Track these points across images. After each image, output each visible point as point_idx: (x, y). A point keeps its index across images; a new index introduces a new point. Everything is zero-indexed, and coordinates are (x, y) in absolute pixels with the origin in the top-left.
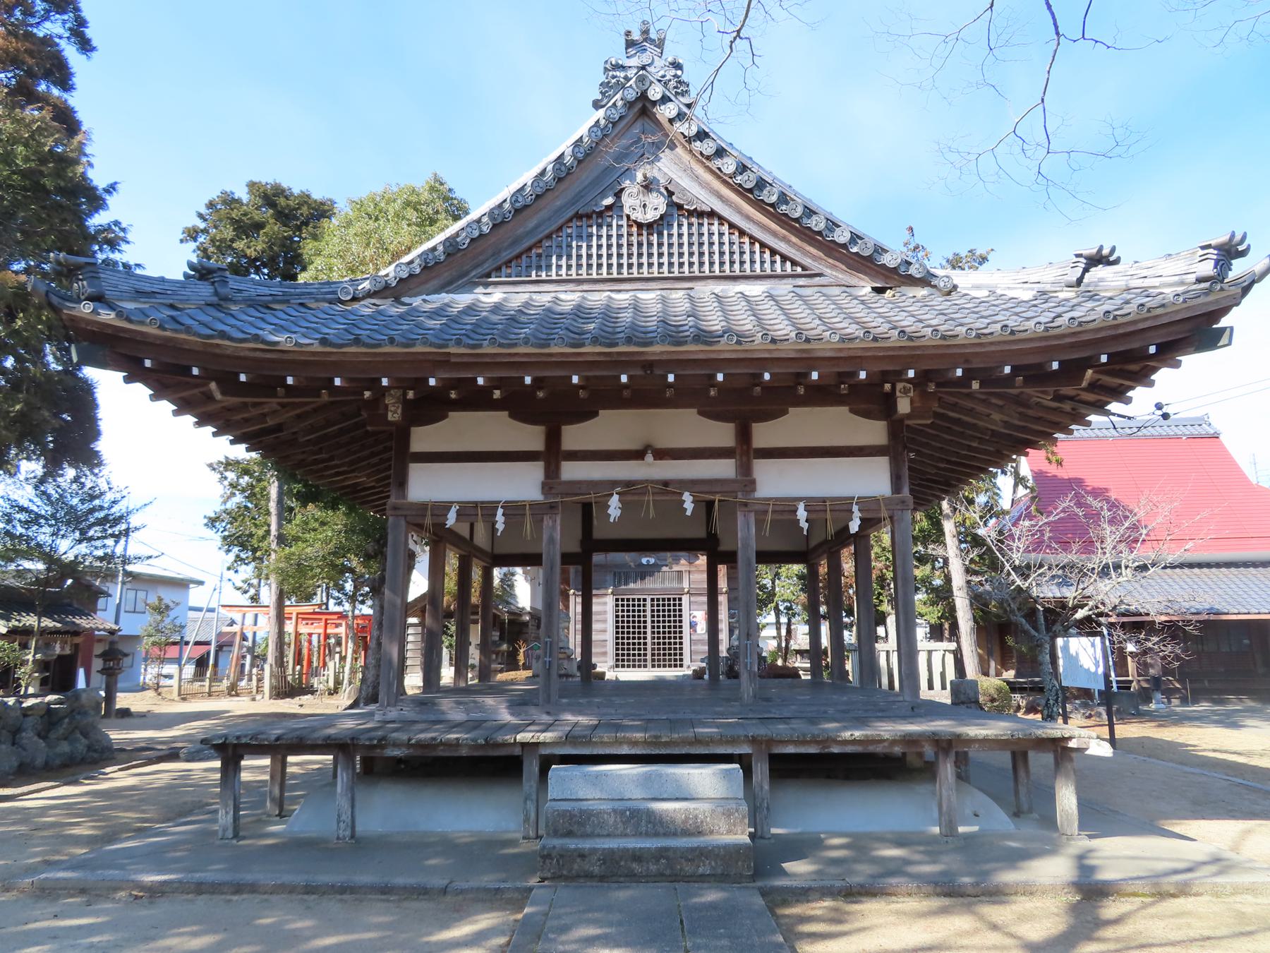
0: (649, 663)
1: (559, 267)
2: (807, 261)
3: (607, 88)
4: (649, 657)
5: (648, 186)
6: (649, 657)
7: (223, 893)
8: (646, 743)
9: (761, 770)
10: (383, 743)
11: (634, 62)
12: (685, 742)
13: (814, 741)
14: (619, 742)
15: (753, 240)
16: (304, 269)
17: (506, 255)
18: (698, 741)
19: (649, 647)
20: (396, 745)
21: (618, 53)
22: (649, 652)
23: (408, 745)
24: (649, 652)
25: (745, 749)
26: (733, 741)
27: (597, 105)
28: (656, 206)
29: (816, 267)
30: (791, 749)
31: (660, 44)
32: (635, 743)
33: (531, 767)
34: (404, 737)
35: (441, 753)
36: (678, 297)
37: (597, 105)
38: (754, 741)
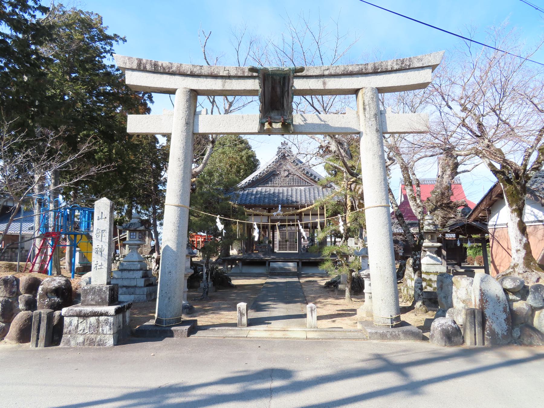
0: (288, 250)
1: (270, 184)
2: (311, 183)
3: (278, 152)
4: (288, 248)
5: (285, 170)
6: (288, 248)
7: (111, 212)
8: (284, 259)
9: (300, 264)
10: (246, 259)
11: (283, 147)
12: (289, 259)
13: (307, 260)
14: (280, 259)
15: (302, 179)
16: (64, 199)
17: (261, 182)
18: (291, 259)
19: (288, 245)
20: (248, 259)
21: (280, 146)
22: (288, 247)
23: (250, 259)
24: (288, 247)
25: (298, 261)
26: (296, 259)
27: (277, 155)
28: (286, 173)
29: (313, 184)
30: (304, 261)
31: (287, 144)
32: (282, 260)
33: (267, 263)
34: (249, 258)
35: (254, 261)
36: (281, 189)
37: (277, 155)
38: (299, 259)
